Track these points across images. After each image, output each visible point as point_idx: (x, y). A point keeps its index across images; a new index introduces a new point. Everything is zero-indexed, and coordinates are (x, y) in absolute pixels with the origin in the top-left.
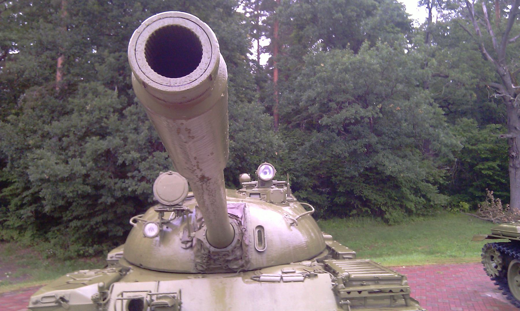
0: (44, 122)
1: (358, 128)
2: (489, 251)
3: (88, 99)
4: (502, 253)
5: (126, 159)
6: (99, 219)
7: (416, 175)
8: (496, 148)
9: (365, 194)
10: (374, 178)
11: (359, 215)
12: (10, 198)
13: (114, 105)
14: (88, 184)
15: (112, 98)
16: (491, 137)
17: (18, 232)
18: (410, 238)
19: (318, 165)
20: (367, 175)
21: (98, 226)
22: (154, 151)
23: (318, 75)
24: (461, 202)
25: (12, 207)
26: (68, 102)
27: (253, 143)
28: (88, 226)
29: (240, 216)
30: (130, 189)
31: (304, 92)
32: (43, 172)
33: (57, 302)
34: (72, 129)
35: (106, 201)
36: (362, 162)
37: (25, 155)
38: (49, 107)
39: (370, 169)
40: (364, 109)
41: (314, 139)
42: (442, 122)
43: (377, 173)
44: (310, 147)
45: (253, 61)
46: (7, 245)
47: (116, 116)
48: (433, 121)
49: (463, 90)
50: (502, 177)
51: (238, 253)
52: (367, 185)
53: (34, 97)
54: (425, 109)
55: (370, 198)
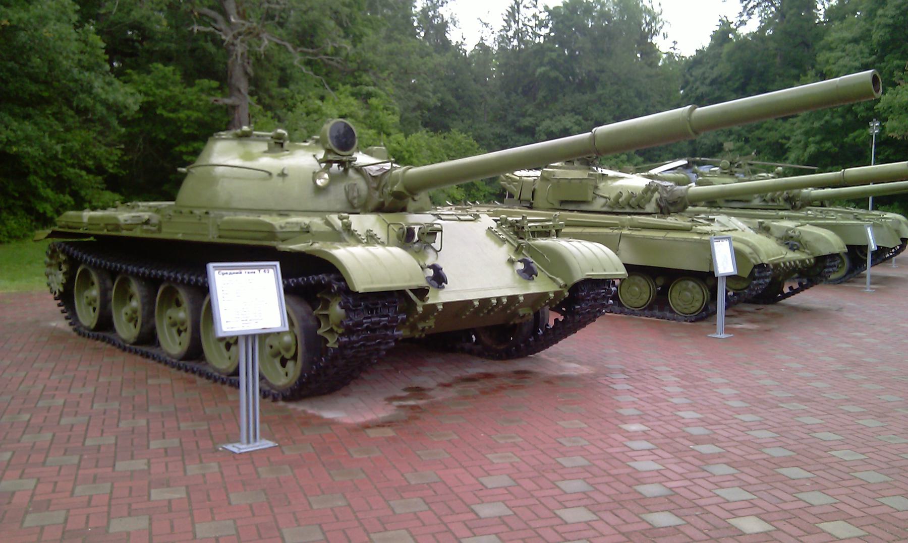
8: (207, 119)
16: (201, 100)
18: (30, 263)
48: (84, 58)
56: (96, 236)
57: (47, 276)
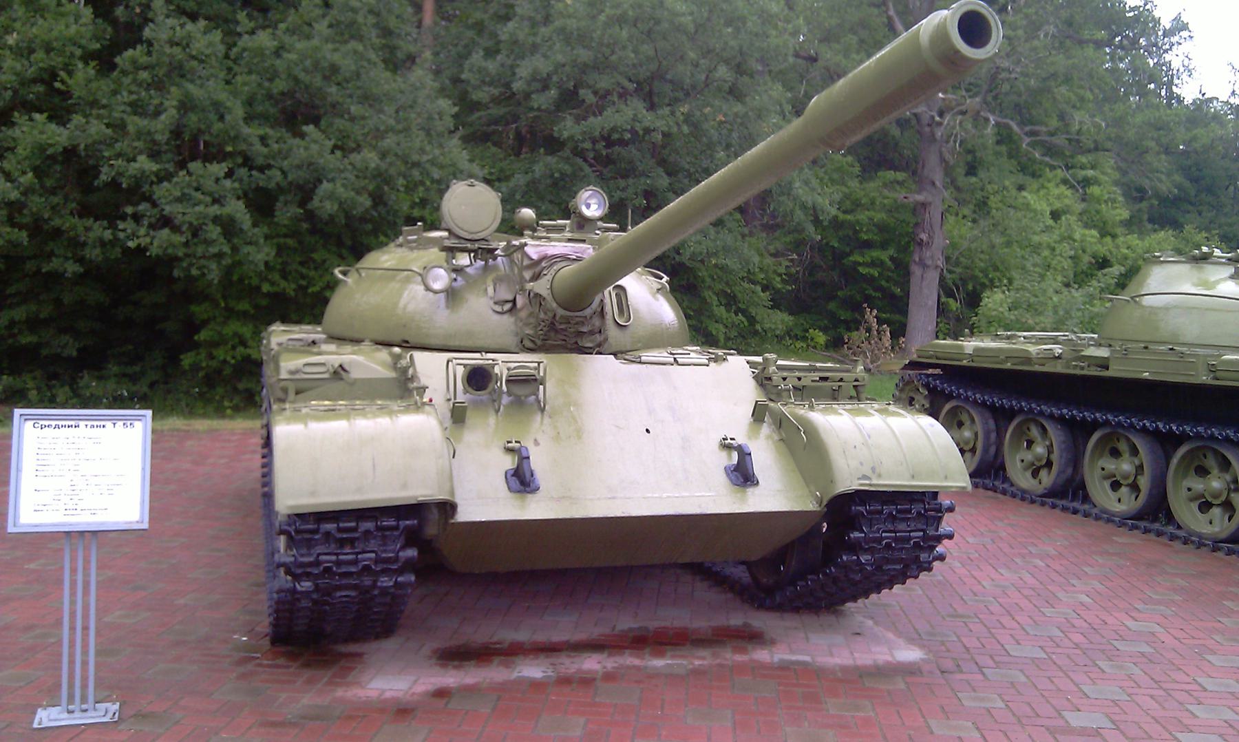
1: (633, 152)
2: (908, 388)
8: (892, 221)
13: (83, 42)
14: (21, 227)
27: (416, 165)
35: (61, 270)
41: (539, 169)
44: (527, 185)
50: (896, 284)
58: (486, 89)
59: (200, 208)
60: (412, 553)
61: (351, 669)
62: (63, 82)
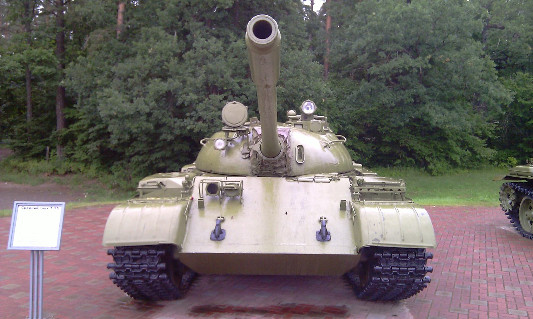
0: (109, 64)
1: (407, 78)
2: (506, 189)
3: (151, 43)
4: (517, 190)
5: (185, 100)
6: (158, 155)
7: (462, 127)
9: (410, 144)
10: (421, 129)
11: (403, 165)
12: (76, 133)
13: (174, 50)
15: (172, 43)
17: (84, 165)
18: (451, 188)
19: (366, 114)
20: (415, 127)
21: (157, 162)
22: (210, 94)
23: (369, 24)
24: (509, 158)
25: (78, 142)
26: (132, 44)
27: (301, 90)
28: (148, 162)
29: (286, 136)
30: (188, 128)
31: (355, 40)
32: (111, 109)
33: (158, 185)
34: (136, 71)
35: (166, 138)
36: (408, 112)
37: (93, 93)
38: (114, 49)
39: (417, 120)
40: (413, 60)
41: (361, 88)
42: (493, 75)
43: (425, 125)
44: (358, 95)
45: (306, 7)
46: (75, 176)
47: (176, 59)
48: (484, 73)
49: (518, 42)
51: (283, 162)
52: (414, 136)
53: (98, 39)
54: (474, 61)
55: (415, 148)
56: (527, 179)
57: (501, 200)
58: (340, 55)
59: (213, 113)
60: (163, 265)
61: (153, 312)
62: (166, 66)
